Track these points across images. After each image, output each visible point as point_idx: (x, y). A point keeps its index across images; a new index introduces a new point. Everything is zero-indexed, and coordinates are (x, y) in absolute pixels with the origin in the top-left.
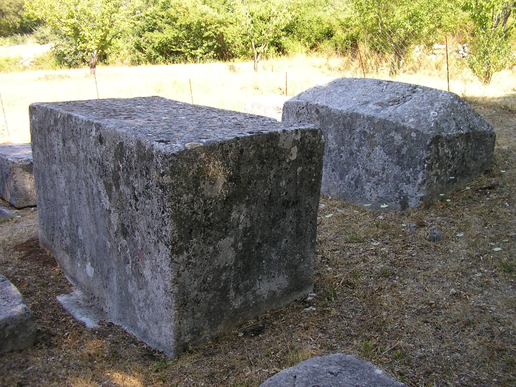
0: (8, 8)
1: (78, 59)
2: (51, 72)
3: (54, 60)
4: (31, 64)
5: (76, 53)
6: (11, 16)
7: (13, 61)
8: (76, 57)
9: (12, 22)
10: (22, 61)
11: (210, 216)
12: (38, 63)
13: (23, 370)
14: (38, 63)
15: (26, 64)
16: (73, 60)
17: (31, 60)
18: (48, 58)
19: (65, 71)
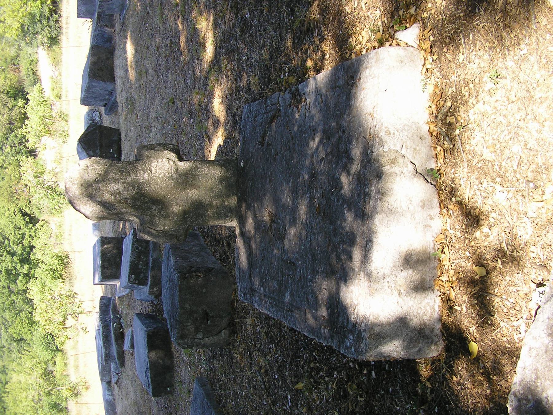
0: (5, 116)
1: (55, 26)
2: (71, 361)
3: (54, 48)
4: (57, 69)
5: (50, 27)
6: (13, 114)
7: (54, 84)
8: (53, 27)
9: (18, 115)
10: (55, 77)
11: (398, 388)
12: (56, 63)
13: (349, 399)
14: (56, 63)
15: (57, 73)
16: (56, 29)
17: (54, 69)
18: (53, 53)
19: (63, 38)
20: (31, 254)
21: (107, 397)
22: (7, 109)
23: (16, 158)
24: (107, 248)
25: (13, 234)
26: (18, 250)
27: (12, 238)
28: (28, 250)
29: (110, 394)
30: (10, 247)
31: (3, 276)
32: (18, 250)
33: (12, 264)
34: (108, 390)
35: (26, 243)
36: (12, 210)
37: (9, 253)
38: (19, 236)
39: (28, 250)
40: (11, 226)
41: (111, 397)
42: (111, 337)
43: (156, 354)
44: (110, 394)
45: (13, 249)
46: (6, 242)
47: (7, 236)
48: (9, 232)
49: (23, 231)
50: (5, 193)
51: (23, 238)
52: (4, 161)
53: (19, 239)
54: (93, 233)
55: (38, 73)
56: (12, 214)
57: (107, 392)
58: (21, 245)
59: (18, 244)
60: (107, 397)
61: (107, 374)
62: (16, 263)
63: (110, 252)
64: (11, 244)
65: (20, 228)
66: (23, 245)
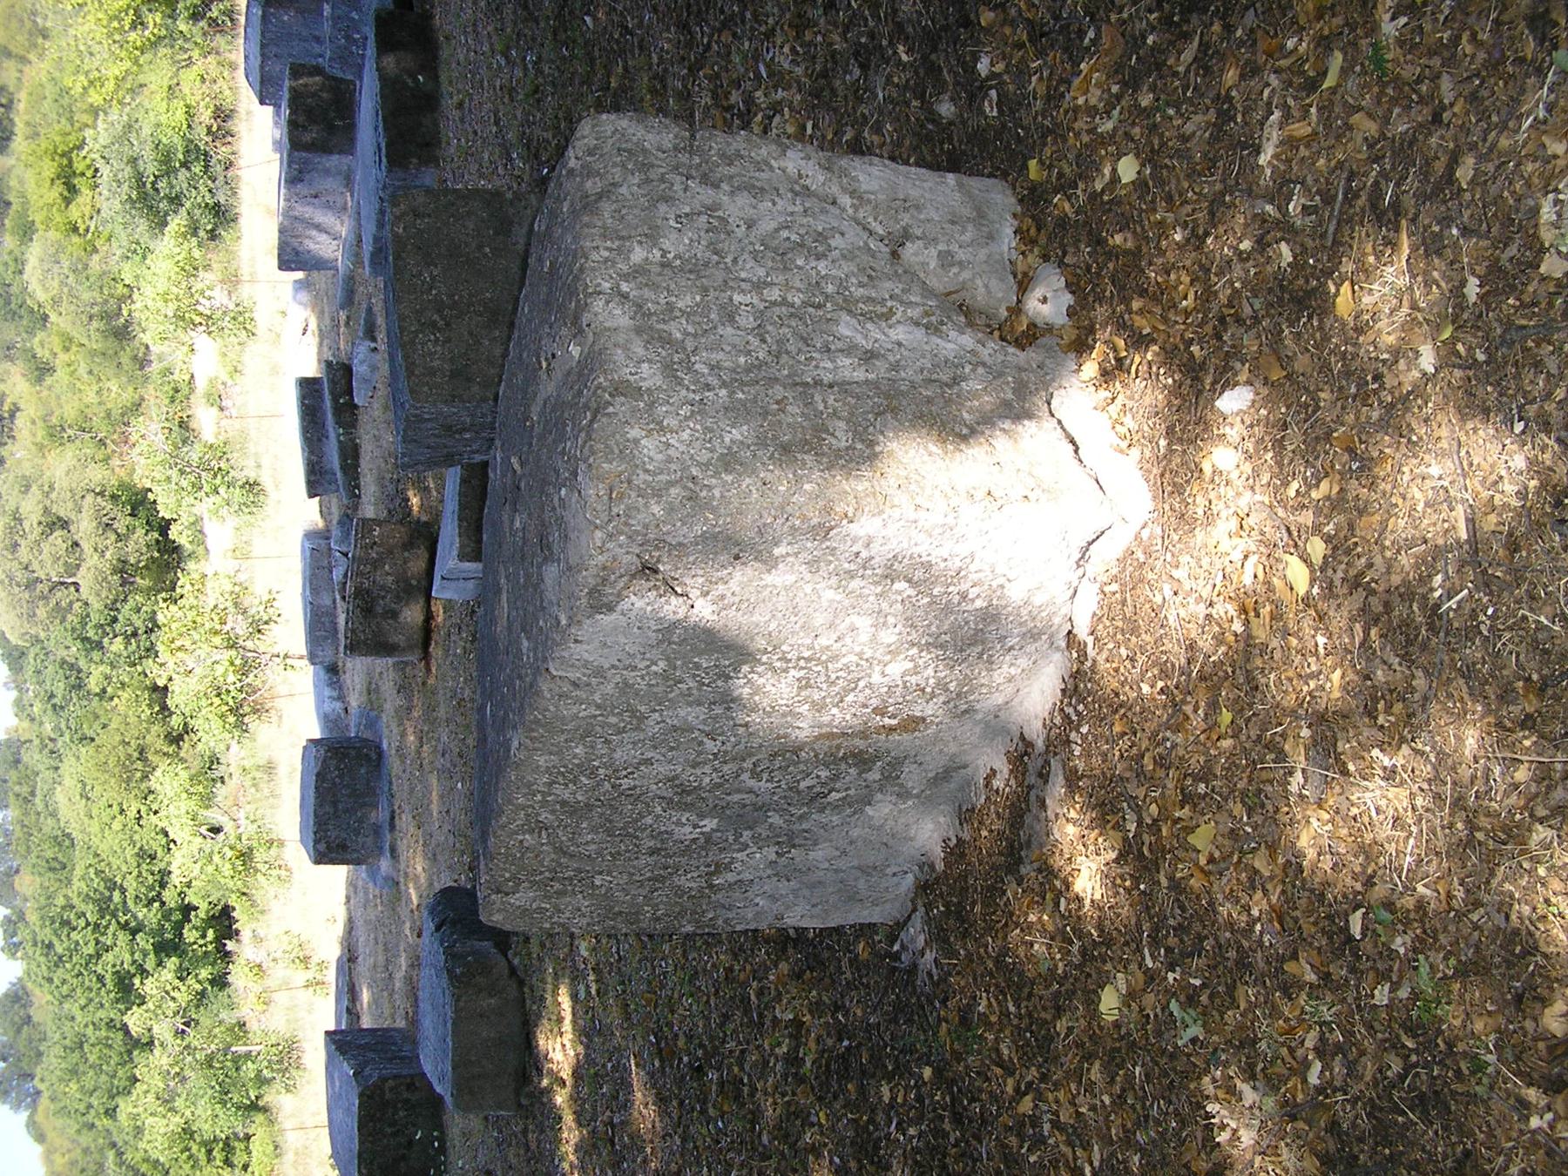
0: (108, 555)
20: (187, 927)
21: (329, 707)
22: (113, 537)
23: (139, 668)
24: (306, 85)
25: (135, 873)
26: (150, 916)
27: (131, 884)
28: (177, 916)
29: (335, 694)
30: (126, 911)
31: (109, 992)
32: (150, 916)
33: (133, 954)
34: (330, 685)
35: (170, 896)
36: (132, 813)
37: (124, 926)
38: (150, 878)
39: (177, 916)
40: (130, 852)
41: (338, 705)
42: (324, 414)
43: (398, 62)
44: (335, 694)
45: (136, 918)
46: (117, 896)
47: (118, 880)
48: (124, 869)
49: (162, 865)
50: (112, 761)
51: (163, 885)
52: (107, 677)
53: (152, 888)
54: (294, 298)
55: (193, 425)
56: (132, 823)
57: (327, 692)
58: (156, 905)
59: (150, 902)
60: (329, 707)
61: (326, 638)
62: (145, 954)
63: (314, 95)
64: (130, 903)
65: (153, 857)
66: (163, 903)
